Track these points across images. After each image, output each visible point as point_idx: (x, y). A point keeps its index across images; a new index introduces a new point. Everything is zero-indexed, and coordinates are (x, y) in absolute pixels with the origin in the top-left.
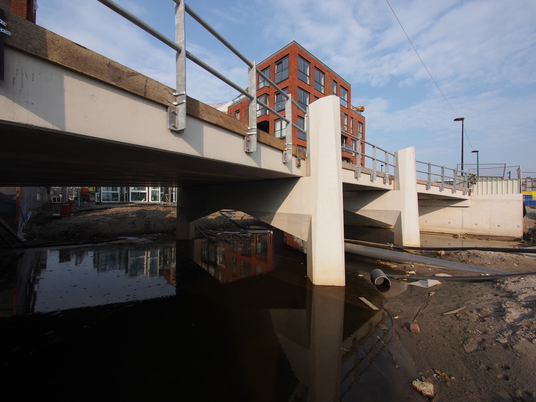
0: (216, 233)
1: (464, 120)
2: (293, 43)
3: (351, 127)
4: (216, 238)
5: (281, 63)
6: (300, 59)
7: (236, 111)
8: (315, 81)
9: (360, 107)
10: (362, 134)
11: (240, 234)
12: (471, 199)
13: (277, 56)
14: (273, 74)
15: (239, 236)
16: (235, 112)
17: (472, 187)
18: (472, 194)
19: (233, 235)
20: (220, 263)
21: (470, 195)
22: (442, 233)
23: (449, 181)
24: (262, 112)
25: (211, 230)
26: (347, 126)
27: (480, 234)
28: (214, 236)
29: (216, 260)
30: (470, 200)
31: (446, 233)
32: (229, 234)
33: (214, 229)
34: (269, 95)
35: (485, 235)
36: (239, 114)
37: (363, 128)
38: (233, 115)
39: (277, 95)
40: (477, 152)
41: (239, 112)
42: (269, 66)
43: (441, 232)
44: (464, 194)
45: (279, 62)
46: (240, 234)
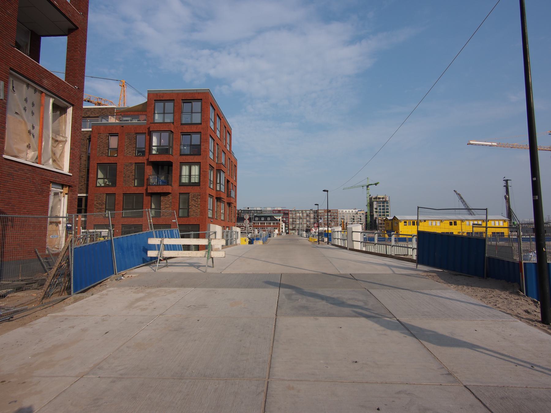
7: (109, 134)
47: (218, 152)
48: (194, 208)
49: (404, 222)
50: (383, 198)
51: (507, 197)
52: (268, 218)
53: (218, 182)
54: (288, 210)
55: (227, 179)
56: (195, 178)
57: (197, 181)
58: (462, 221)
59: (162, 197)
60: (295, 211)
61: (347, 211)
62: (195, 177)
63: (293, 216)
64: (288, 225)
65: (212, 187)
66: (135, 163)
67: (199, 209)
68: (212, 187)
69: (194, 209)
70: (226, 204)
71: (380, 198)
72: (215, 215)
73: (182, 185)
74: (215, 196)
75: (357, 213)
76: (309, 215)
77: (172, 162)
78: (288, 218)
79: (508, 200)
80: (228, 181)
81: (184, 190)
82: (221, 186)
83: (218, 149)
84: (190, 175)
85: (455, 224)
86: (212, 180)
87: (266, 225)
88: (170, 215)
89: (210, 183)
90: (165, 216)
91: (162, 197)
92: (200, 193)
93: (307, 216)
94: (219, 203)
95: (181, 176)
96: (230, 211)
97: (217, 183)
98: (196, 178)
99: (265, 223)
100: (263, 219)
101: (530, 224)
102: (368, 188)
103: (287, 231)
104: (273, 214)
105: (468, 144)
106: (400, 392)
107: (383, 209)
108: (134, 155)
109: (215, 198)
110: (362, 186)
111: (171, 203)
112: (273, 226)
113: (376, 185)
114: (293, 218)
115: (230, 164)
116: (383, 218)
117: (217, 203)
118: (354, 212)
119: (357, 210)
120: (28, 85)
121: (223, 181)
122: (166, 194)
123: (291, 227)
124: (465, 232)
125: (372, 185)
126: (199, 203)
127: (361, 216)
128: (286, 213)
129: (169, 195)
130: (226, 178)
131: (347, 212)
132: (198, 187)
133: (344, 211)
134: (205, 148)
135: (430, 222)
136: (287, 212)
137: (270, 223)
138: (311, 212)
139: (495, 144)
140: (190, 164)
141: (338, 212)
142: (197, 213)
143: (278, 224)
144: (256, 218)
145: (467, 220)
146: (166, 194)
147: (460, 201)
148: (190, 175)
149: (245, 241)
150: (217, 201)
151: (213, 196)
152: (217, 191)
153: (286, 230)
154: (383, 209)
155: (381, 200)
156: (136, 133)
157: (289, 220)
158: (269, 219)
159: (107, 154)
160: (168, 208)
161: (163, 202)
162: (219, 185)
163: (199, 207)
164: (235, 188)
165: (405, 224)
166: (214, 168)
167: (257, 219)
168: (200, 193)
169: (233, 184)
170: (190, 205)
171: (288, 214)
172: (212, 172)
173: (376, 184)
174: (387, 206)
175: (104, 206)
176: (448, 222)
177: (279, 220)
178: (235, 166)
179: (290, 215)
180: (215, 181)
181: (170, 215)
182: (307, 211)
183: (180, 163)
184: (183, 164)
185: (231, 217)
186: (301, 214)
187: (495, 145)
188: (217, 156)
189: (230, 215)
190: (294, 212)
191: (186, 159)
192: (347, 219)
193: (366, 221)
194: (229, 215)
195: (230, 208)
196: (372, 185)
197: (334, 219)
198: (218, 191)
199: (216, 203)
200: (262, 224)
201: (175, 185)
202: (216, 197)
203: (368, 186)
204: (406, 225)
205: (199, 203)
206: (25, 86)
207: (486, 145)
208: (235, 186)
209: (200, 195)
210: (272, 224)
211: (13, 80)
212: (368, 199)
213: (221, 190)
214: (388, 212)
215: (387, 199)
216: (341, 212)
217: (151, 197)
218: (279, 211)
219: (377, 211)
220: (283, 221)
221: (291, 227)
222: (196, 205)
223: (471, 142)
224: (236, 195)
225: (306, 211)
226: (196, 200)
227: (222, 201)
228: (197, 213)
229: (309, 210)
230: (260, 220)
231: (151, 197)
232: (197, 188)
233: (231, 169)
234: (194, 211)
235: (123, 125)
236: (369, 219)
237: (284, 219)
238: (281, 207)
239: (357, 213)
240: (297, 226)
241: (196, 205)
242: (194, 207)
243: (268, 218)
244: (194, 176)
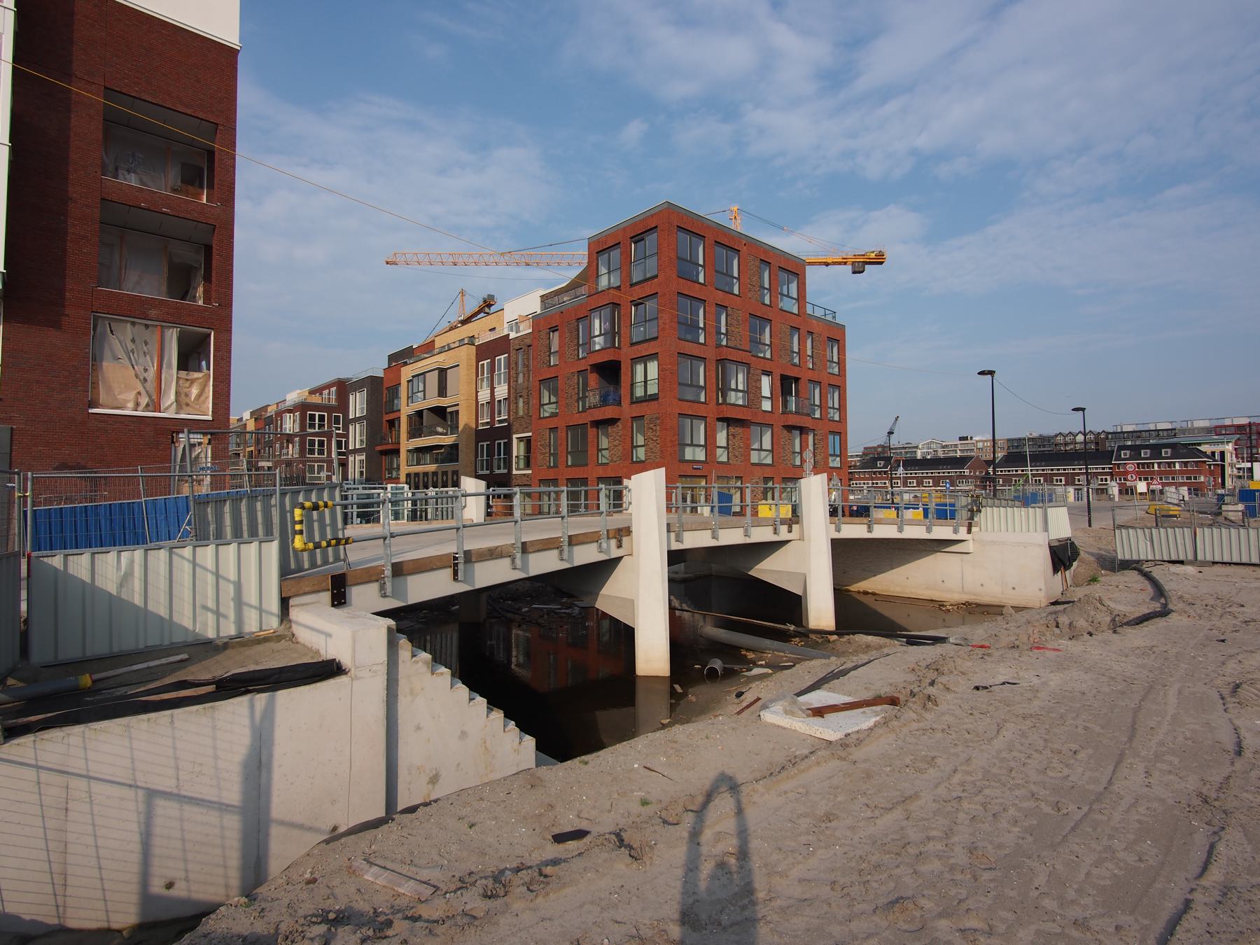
0: (519, 609)
1: (996, 376)
2: (666, 206)
3: (809, 353)
4: (523, 619)
5: (643, 239)
6: (681, 235)
7: (550, 329)
8: (716, 271)
9: (873, 252)
10: (838, 363)
11: (560, 609)
12: (973, 540)
13: (635, 225)
14: (626, 262)
15: (560, 612)
16: (548, 330)
17: (978, 516)
18: (974, 529)
19: (550, 612)
20: (518, 665)
21: (969, 531)
22: (932, 600)
23: (1154, 429)
24: (605, 342)
25: (510, 602)
26: (799, 353)
27: (987, 603)
28: (517, 614)
29: (510, 662)
30: (971, 541)
31: (938, 600)
32: (541, 609)
33: (513, 599)
34: (619, 305)
35: (994, 603)
36: (557, 334)
37: (842, 351)
38: (543, 333)
39: (636, 305)
40: (1083, 410)
41: (557, 330)
42: (620, 243)
43: (930, 598)
44: (956, 531)
45: (638, 238)
46: (560, 609)
66: (578, 372)
67: (658, 446)
73: (635, 401)
81: (637, 410)
99: (1153, 464)
101: (684, 457)
106: (311, 828)
108: (576, 357)
112: (1181, 472)
120: (133, 324)
140: (645, 359)
144: (1122, 452)
156: (578, 319)
159: (548, 364)
175: (548, 450)
183: (631, 359)
184: (635, 360)
201: (625, 402)
206: (129, 325)
211: (110, 324)
217: (597, 428)
226: (654, 428)
230: (1159, 456)
231: (597, 428)
235: (561, 309)
238: (1249, 417)
241: (655, 439)
243: (1163, 451)
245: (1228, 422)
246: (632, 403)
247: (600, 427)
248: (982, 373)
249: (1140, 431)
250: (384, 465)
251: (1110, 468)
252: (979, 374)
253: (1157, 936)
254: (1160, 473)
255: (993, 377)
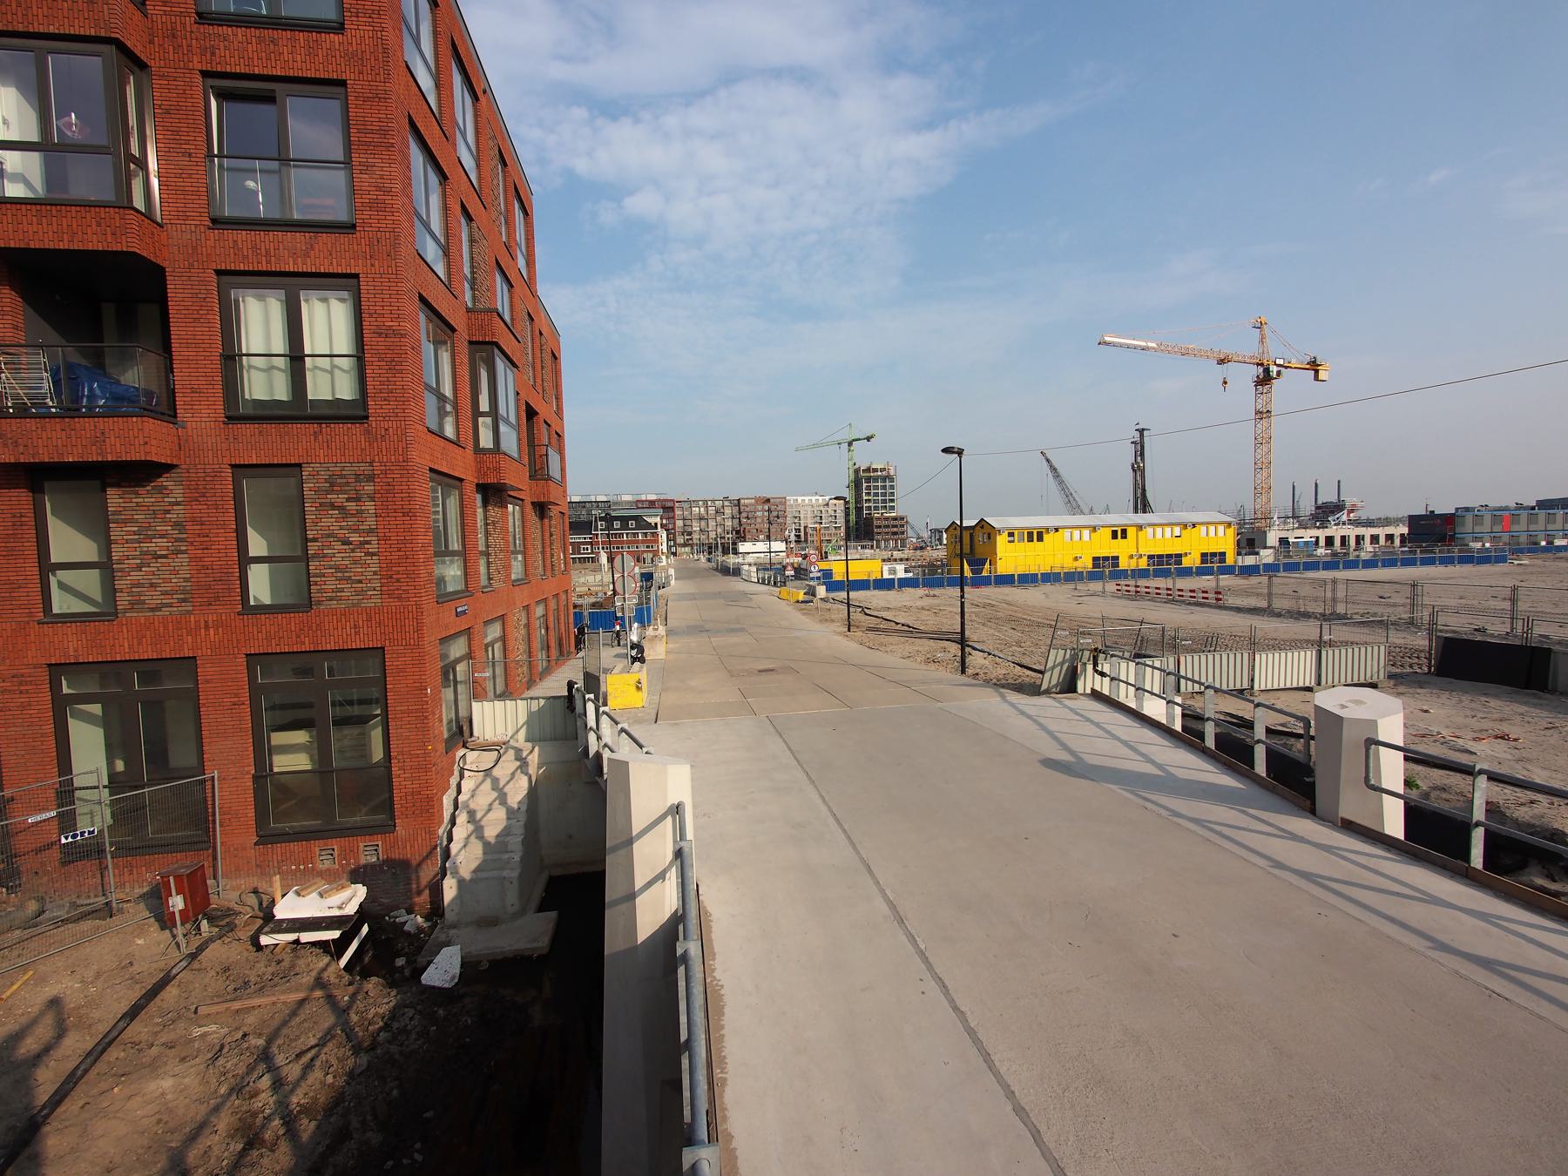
47: (472, 258)
48: (339, 555)
49: (1009, 533)
50: (882, 470)
51: (1142, 465)
52: (630, 522)
53: (484, 406)
54: (673, 500)
55: (527, 404)
56: (331, 373)
57: (345, 390)
58: (1140, 527)
59: (110, 491)
60: (688, 501)
61: (807, 498)
62: (334, 366)
63: (686, 513)
64: (674, 534)
65: (449, 431)
68: (449, 431)
69: (338, 560)
70: (529, 509)
71: (875, 470)
72: (478, 573)
73: (240, 414)
74: (471, 478)
75: (827, 505)
76: (722, 510)
77: (162, 270)
78: (674, 517)
79: (1138, 470)
80: (531, 413)
81: (259, 445)
82: (503, 428)
83: (472, 241)
84: (296, 356)
85: (1124, 534)
86: (448, 391)
87: (625, 538)
88: (184, 600)
89: (442, 414)
90: (153, 610)
91: (110, 491)
92: (371, 463)
93: (717, 512)
94: (494, 512)
95: (231, 358)
96: (547, 535)
97: (477, 414)
98: (337, 372)
99: (623, 534)
100: (617, 524)
102: (852, 448)
103: (673, 549)
104: (639, 511)
105: (1100, 344)
107: (884, 494)
109: (469, 488)
110: (839, 444)
111: (177, 525)
112: (643, 542)
113: (868, 441)
114: (684, 519)
115: (533, 343)
116: (882, 513)
117: (485, 511)
118: (820, 501)
119: (827, 498)
121: (508, 407)
122: (140, 473)
123: (680, 540)
124: (1145, 555)
125: (859, 439)
126: (371, 522)
127: (835, 511)
128: (668, 508)
129: (164, 481)
130: (522, 395)
131: (807, 501)
132: (357, 429)
133: (800, 501)
134: (379, 189)
135: (1067, 533)
136: (670, 504)
137: (635, 535)
138: (726, 503)
139: (1154, 345)
141: (785, 502)
142: (360, 582)
143: (655, 535)
145: (1150, 525)
146: (140, 473)
147: (1050, 475)
148: (296, 356)
149: (639, 688)
150: (485, 503)
151: (461, 480)
152: (478, 450)
153: (669, 547)
154: (884, 494)
155: (879, 473)
157: (674, 524)
158: (632, 524)
160: (165, 557)
161: (125, 522)
162: (489, 420)
163: (373, 548)
164: (558, 441)
165: (1011, 538)
166: (453, 330)
167: (602, 525)
168: (371, 463)
169: (549, 426)
170: (315, 540)
171: (672, 509)
172: (445, 357)
173: (868, 439)
174: (892, 487)
176: (1108, 532)
177: (656, 524)
178: (555, 357)
179: (678, 512)
180: (466, 403)
181: (184, 600)
182: (717, 502)
185: (552, 555)
186: (702, 509)
187: (1154, 348)
188: (467, 270)
189: (548, 549)
190: (686, 505)
191: (255, 248)
192: (806, 518)
193: (847, 521)
194: (543, 552)
195: (546, 521)
196: (859, 439)
197: (778, 517)
198: (485, 451)
199: (480, 511)
200: (620, 537)
202: (476, 481)
203: (850, 444)
204: (1013, 541)
205: (371, 522)
207: (1135, 347)
208: (559, 436)
209: (371, 478)
210: (640, 538)
212: (851, 471)
213: (504, 446)
214: (892, 501)
215: (892, 473)
216: (792, 502)
218: (652, 504)
219: (870, 498)
220: (663, 526)
221: (680, 540)
222: (355, 538)
223: (1108, 339)
224: (563, 470)
225: (713, 501)
226: (352, 506)
227: (509, 499)
228: (360, 582)
229: (722, 498)
232: (352, 433)
233: (538, 361)
234: (338, 569)
236: (853, 517)
237: (664, 522)
239: (827, 505)
240: (695, 536)
241: (355, 538)
242: (338, 546)
243: (630, 522)
244: (324, 363)
245: (643, 498)
246: (233, 418)
247: (47, 485)
248: (947, 450)
249: (585, 502)
250: (155, 182)
251: (590, 538)
252: (943, 451)
253: (722, 992)
254: (628, 542)
255: (960, 457)
